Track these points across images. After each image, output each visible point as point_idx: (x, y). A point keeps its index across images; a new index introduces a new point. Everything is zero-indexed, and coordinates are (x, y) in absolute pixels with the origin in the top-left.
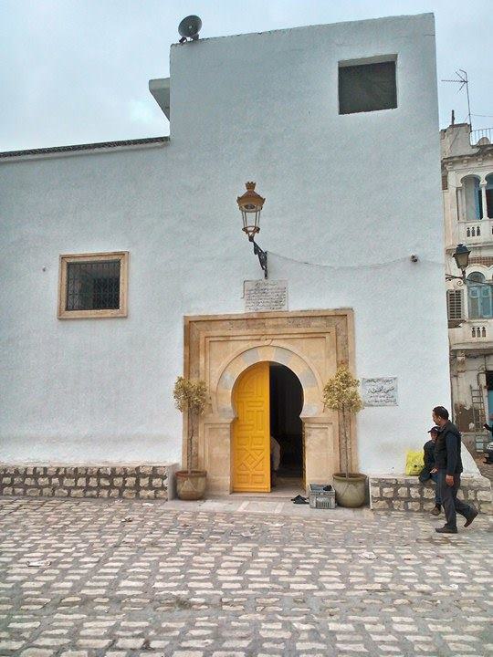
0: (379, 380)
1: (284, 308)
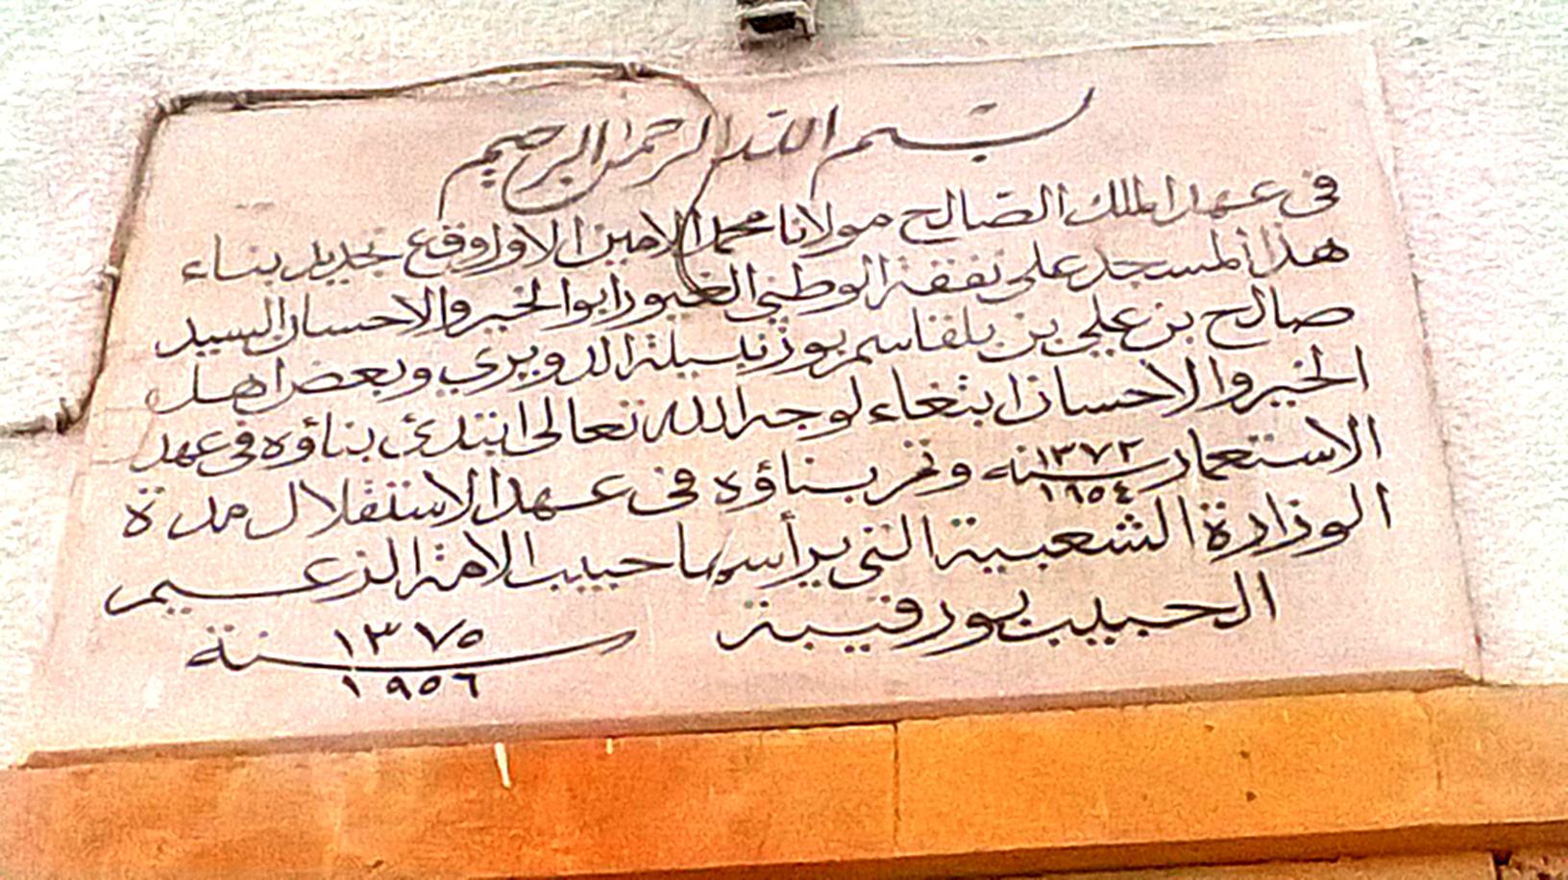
1: (1371, 609)
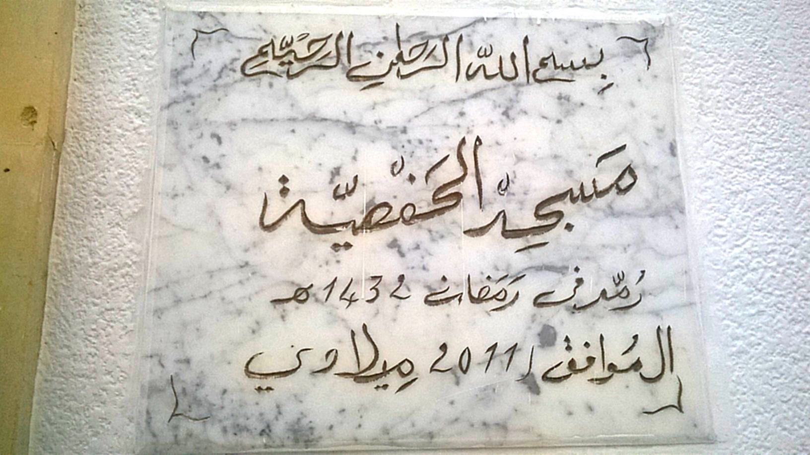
0: (416, 51)
